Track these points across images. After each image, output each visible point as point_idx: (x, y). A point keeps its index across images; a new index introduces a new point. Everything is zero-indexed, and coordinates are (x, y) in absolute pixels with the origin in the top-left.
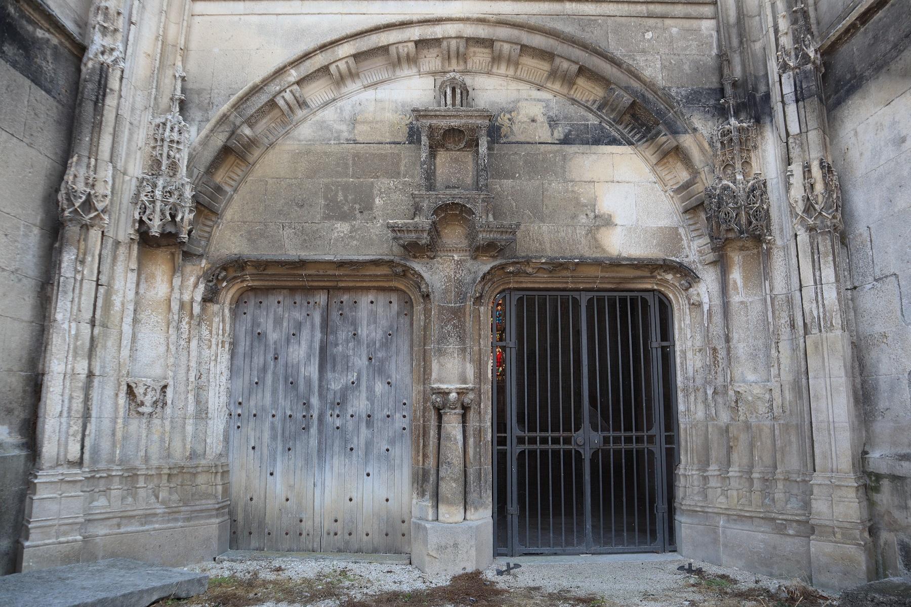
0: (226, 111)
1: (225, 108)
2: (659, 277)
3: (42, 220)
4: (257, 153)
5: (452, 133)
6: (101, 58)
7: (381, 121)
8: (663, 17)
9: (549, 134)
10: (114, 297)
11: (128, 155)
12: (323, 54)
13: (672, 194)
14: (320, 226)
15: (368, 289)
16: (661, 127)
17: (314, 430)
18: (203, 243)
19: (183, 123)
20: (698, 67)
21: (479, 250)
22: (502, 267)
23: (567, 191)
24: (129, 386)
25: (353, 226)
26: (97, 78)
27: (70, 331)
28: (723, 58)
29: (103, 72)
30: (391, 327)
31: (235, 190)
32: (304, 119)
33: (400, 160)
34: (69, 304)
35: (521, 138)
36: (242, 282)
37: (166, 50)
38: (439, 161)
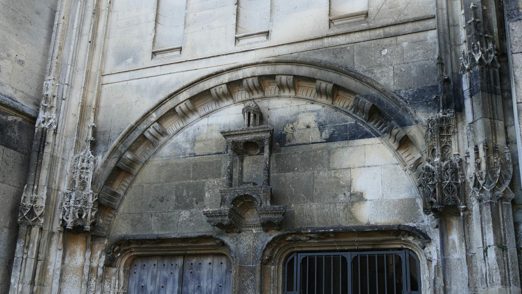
0: (115, 145)
2: (403, 239)
3: (10, 224)
4: (138, 168)
6: (43, 125)
7: (211, 139)
8: (396, 35)
9: (319, 136)
10: (49, 267)
11: (60, 178)
12: (171, 100)
13: (409, 172)
14: (172, 214)
16: (393, 122)
18: (106, 229)
19: (91, 155)
20: (423, 71)
21: (267, 226)
22: (282, 238)
23: (330, 177)
25: (192, 213)
26: (39, 137)
27: (18, 289)
28: (441, 63)
29: (44, 133)
30: (221, 281)
31: (125, 193)
32: (165, 143)
33: (222, 165)
34: (18, 273)
35: (300, 141)
36: (130, 252)
38: (245, 163)
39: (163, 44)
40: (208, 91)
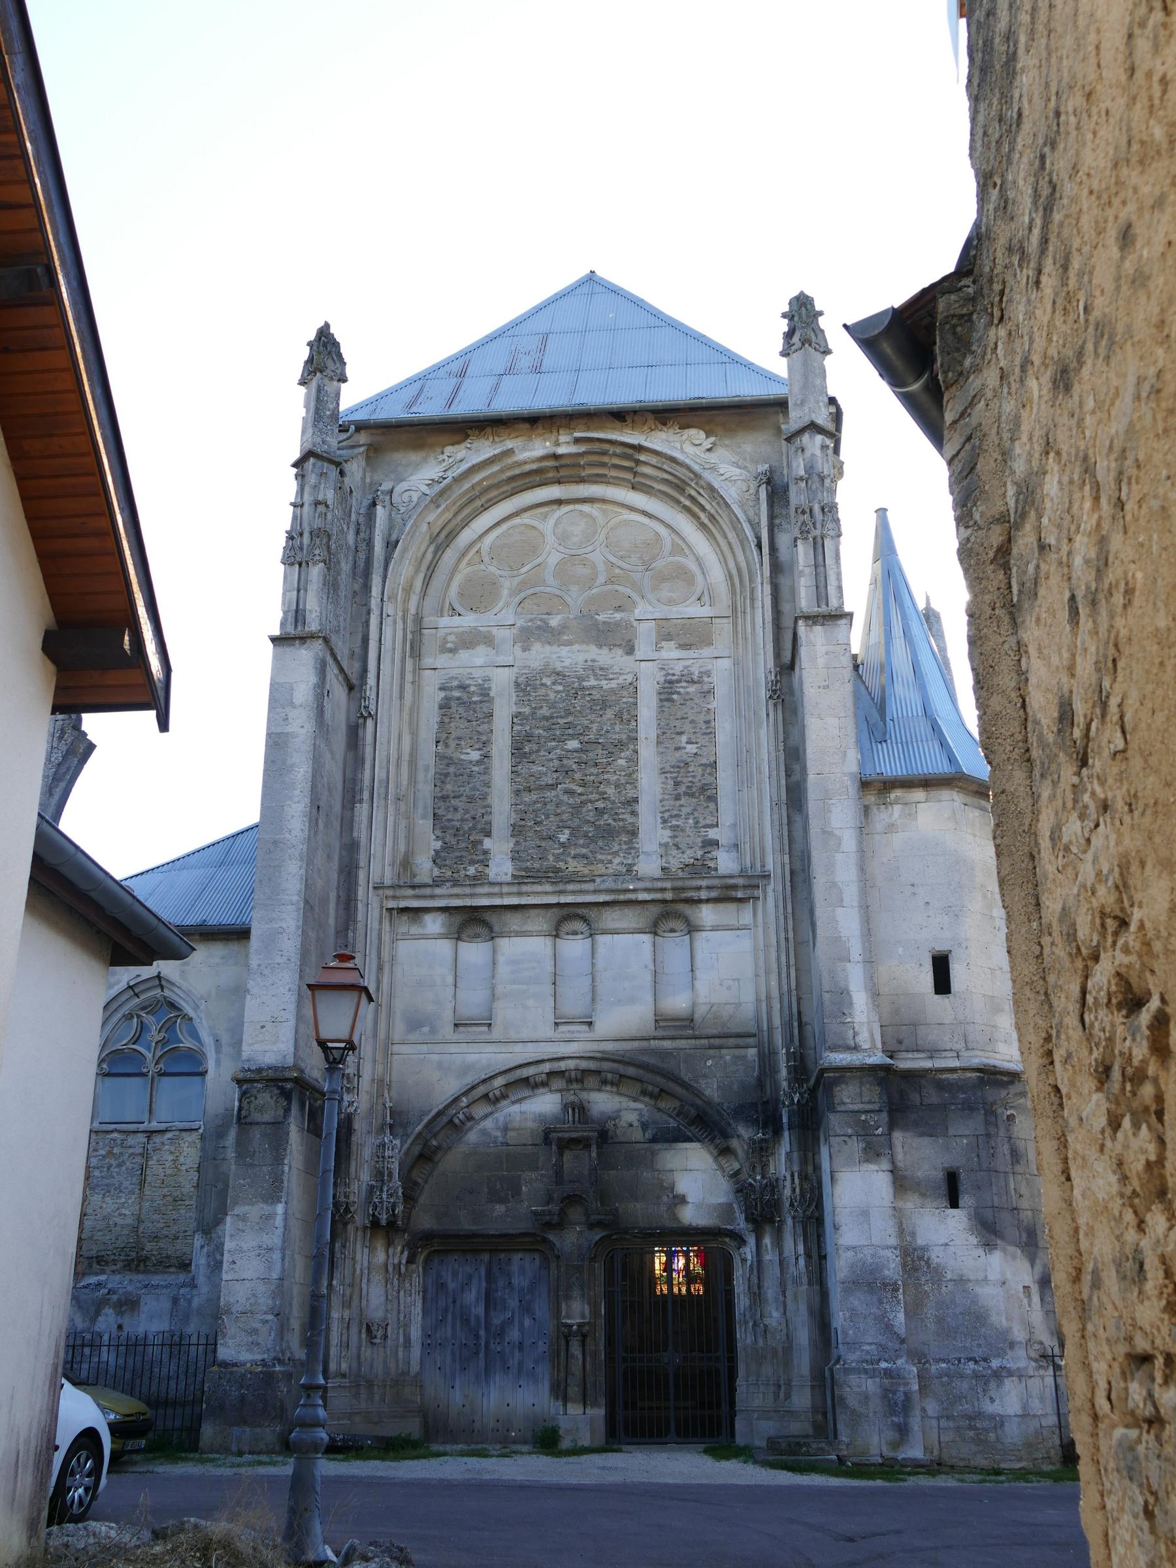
1: (420, 1127)
4: (439, 1155)
5: (576, 1141)
8: (720, 1047)
15: (518, 1250)
17: (482, 1355)
22: (609, 1236)
24: (367, 1325)
28: (760, 1084)
31: (426, 1182)
32: (471, 1128)
35: (622, 1139)
37: (381, 1084)
39: (466, 1012)
40: (527, 1079)
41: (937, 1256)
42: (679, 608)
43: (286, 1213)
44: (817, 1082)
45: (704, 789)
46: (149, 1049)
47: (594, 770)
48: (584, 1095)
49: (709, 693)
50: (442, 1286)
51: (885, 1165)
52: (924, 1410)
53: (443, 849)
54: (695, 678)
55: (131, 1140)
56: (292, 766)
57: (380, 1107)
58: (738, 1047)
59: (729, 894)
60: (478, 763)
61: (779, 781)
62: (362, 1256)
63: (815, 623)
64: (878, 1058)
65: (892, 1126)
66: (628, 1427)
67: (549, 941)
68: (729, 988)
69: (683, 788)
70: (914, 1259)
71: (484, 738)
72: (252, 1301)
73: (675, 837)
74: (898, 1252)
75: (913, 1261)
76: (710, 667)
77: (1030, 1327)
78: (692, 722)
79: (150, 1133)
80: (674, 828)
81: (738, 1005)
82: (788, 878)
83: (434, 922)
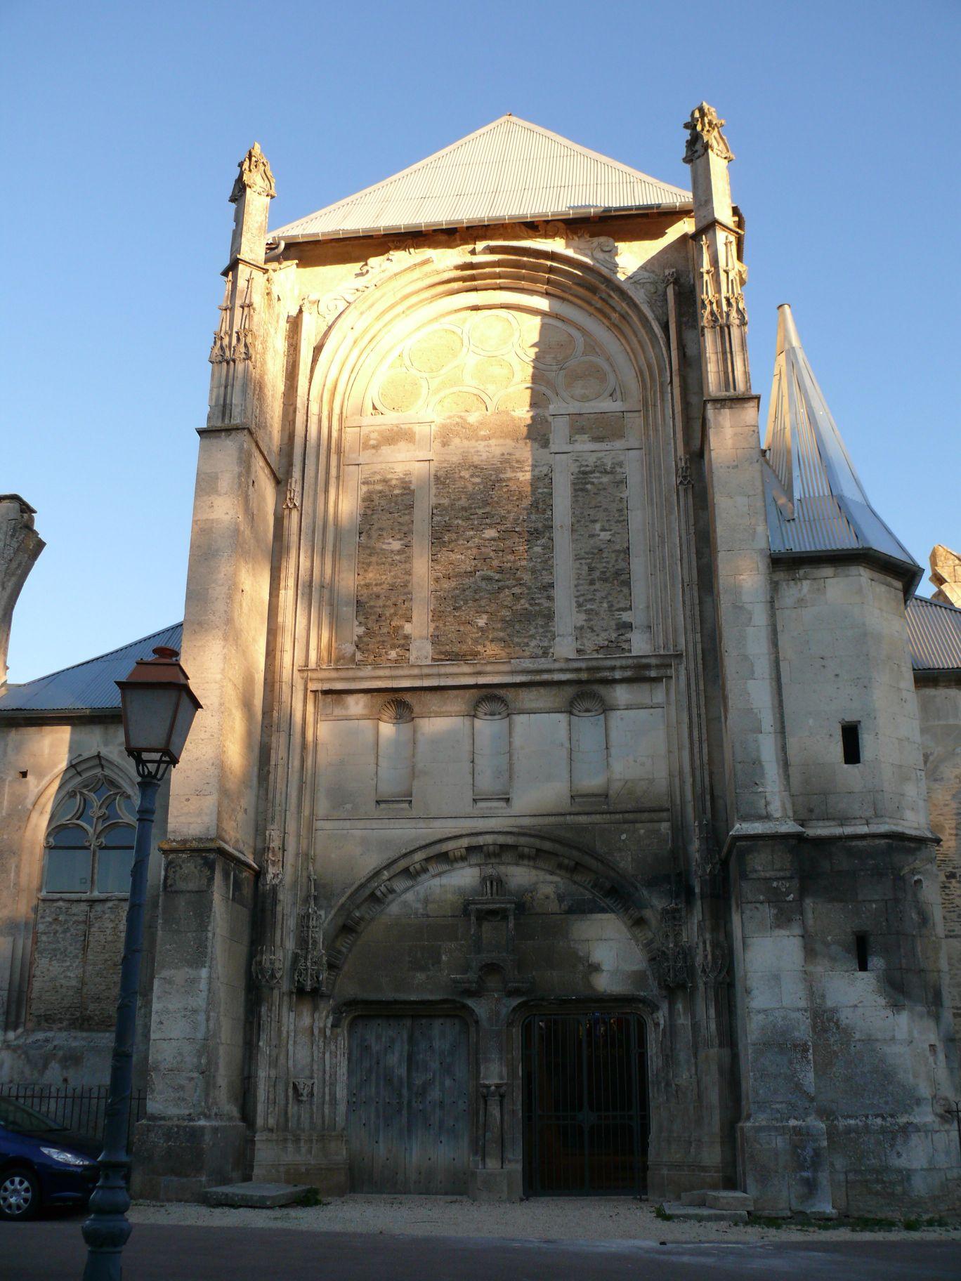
1: (342, 900)
5: (493, 913)
15: (440, 1016)
17: (405, 1112)
24: (295, 1086)
31: (350, 951)
37: (307, 857)
38: (484, 929)
41: (846, 1017)
42: (592, 404)
43: (210, 978)
44: (730, 852)
45: (618, 573)
46: (90, 824)
47: (511, 557)
48: (502, 869)
49: (622, 482)
50: (368, 1048)
51: (797, 930)
52: (832, 1165)
53: (366, 634)
54: (608, 469)
55: (75, 909)
56: (217, 551)
57: (305, 880)
58: (651, 821)
59: (640, 675)
60: (400, 552)
61: (690, 563)
62: (288, 1019)
63: (723, 407)
64: (790, 827)
65: (803, 893)
66: (544, 1179)
67: (467, 721)
68: (643, 764)
69: (597, 574)
70: (824, 1019)
71: (405, 529)
72: (179, 1059)
73: (590, 620)
74: (808, 1014)
75: (823, 1022)
76: (622, 458)
77: (934, 1083)
78: (606, 510)
79: (92, 902)
80: (588, 612)
81: (651, 781)
82: (700, 656)
83: (357, 703)
